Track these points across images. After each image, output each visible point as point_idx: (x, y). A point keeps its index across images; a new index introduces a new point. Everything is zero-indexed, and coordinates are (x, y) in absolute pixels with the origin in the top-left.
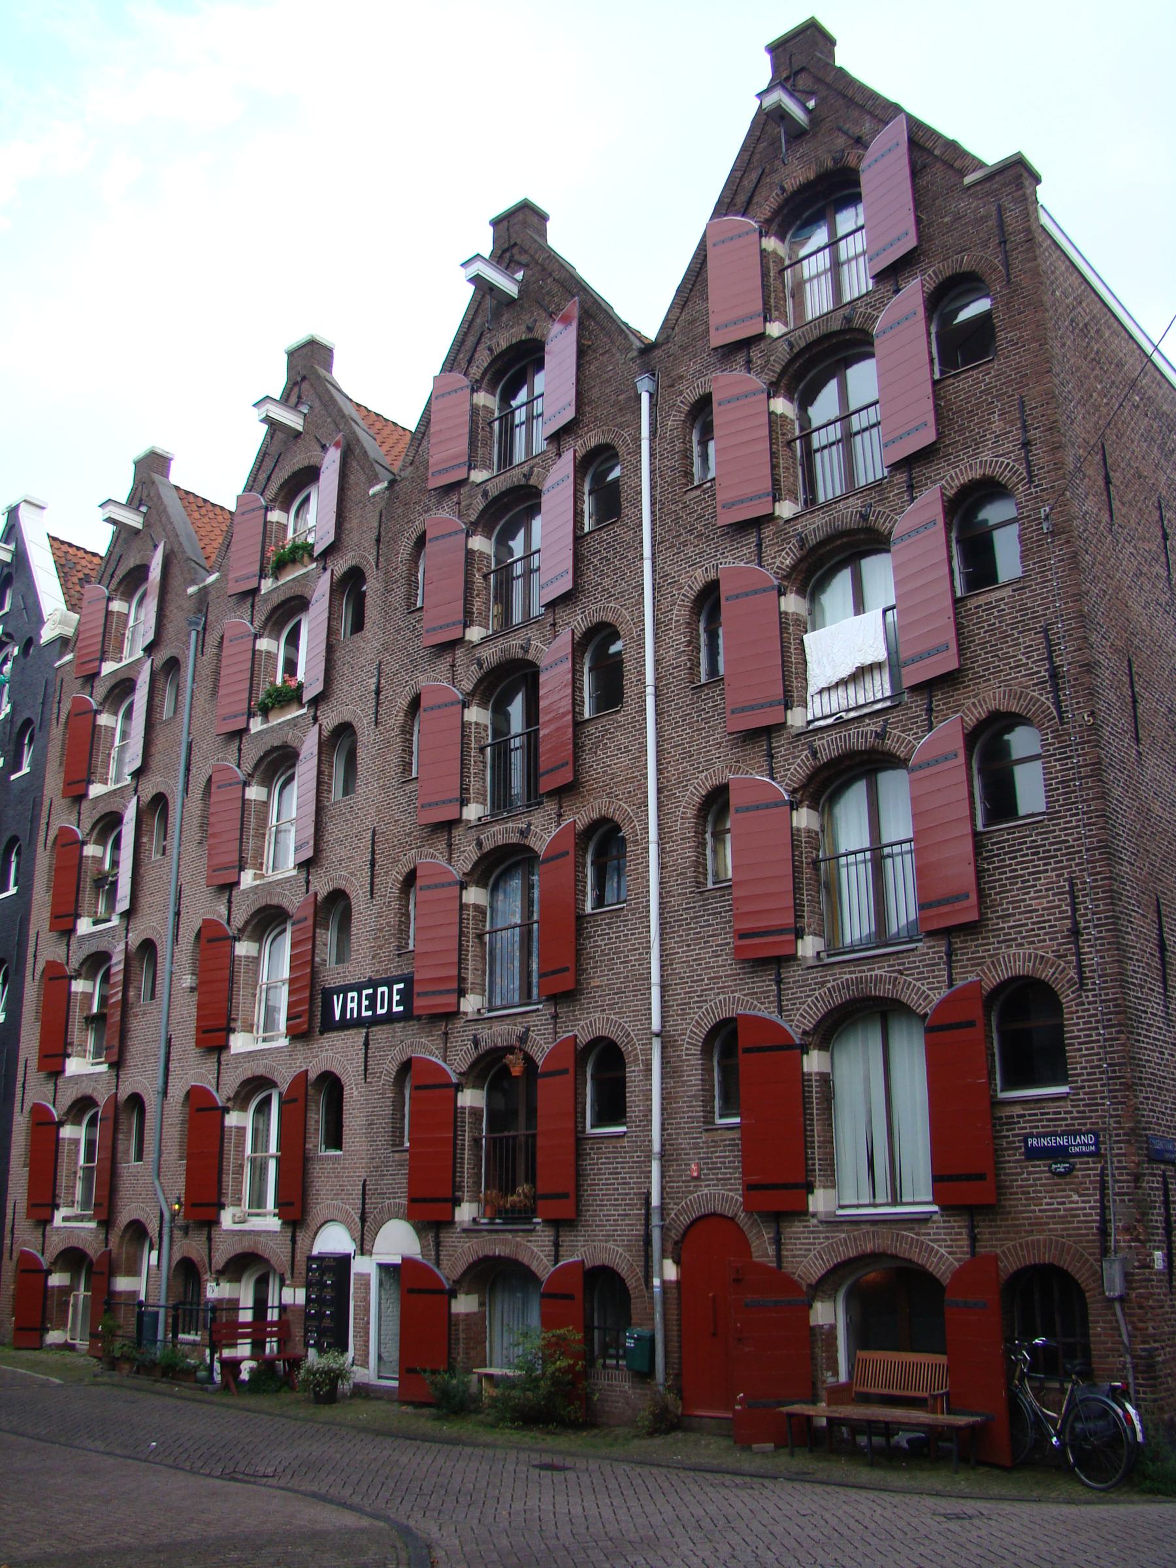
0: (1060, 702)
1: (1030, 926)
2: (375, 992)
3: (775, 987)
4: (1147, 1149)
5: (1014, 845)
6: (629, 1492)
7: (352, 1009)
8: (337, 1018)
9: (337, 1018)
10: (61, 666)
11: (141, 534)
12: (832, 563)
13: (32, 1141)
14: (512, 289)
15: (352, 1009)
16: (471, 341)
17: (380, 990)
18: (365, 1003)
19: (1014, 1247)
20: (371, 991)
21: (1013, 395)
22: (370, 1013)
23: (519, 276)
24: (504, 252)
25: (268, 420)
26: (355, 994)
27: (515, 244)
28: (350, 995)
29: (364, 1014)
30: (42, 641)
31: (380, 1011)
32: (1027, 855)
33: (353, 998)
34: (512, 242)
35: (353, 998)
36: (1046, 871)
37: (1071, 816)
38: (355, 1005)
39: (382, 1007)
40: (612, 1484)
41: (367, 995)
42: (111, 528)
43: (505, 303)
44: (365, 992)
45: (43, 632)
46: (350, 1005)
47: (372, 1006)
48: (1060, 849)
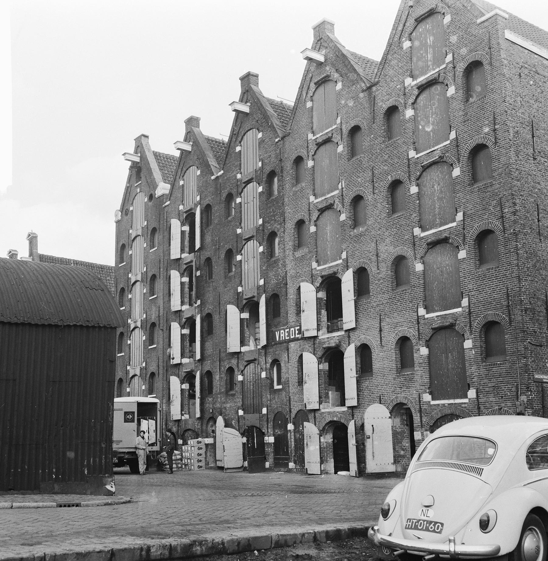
0: (504, 226)
1: (495, 304)
2: (290, 330)
3: (417, 325)
4: (533, 378)
5: (490, 276)
6: (59, 283)
7: (282, 337)
8: (278, 340)
9: (278, 340)
10: (166, 206)
11: (192, 153)
12: (22, 504)
13: (11, 560)
14: (321, 59)
15: (282, 337)
16: (308, 79)
17: (291, 329)
18: (287, 334)
19: (491, 411)
20: (288, 330)
21: (491, 111)
22: (288, 338)
23: (324, 52)
24: (318, 41)
25: (235, 110)
26: (283, 331)
27: (322, 38)
28: (281, 331)
29: (286, 338)
30: (156, 196)
31: (292, 337)
32: (494, 280)
33: (282, 333)
34: (321, 38)
35: (282, 333)
36: (500, 285)
37: (508, 266)
38: (283, 335)
39: (292, 336)
40: (50, 276)
41: (287, 331)
42: (179, 151)
43: (320, 64)
44: (286, 330)
45: (156, 192)
46: (281, 335)
47: (289, 335)
48: (504, 277)
